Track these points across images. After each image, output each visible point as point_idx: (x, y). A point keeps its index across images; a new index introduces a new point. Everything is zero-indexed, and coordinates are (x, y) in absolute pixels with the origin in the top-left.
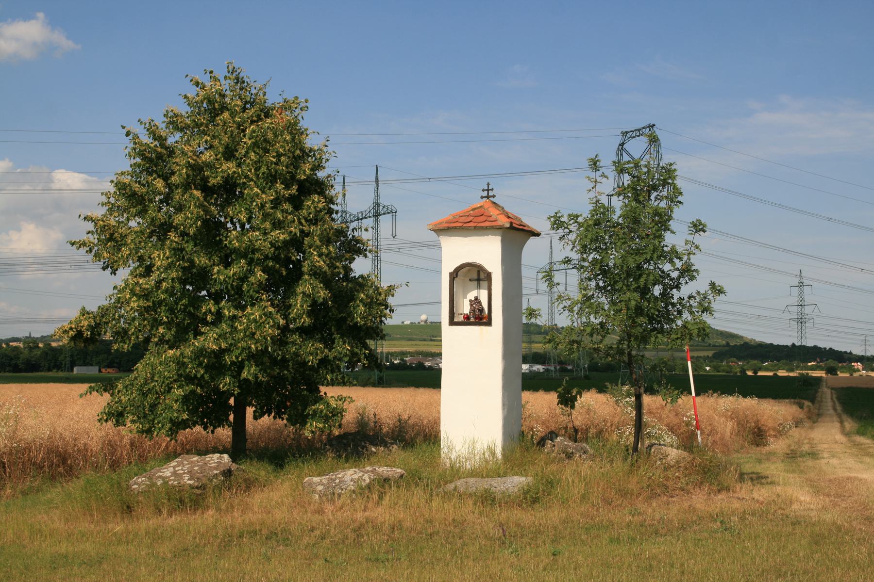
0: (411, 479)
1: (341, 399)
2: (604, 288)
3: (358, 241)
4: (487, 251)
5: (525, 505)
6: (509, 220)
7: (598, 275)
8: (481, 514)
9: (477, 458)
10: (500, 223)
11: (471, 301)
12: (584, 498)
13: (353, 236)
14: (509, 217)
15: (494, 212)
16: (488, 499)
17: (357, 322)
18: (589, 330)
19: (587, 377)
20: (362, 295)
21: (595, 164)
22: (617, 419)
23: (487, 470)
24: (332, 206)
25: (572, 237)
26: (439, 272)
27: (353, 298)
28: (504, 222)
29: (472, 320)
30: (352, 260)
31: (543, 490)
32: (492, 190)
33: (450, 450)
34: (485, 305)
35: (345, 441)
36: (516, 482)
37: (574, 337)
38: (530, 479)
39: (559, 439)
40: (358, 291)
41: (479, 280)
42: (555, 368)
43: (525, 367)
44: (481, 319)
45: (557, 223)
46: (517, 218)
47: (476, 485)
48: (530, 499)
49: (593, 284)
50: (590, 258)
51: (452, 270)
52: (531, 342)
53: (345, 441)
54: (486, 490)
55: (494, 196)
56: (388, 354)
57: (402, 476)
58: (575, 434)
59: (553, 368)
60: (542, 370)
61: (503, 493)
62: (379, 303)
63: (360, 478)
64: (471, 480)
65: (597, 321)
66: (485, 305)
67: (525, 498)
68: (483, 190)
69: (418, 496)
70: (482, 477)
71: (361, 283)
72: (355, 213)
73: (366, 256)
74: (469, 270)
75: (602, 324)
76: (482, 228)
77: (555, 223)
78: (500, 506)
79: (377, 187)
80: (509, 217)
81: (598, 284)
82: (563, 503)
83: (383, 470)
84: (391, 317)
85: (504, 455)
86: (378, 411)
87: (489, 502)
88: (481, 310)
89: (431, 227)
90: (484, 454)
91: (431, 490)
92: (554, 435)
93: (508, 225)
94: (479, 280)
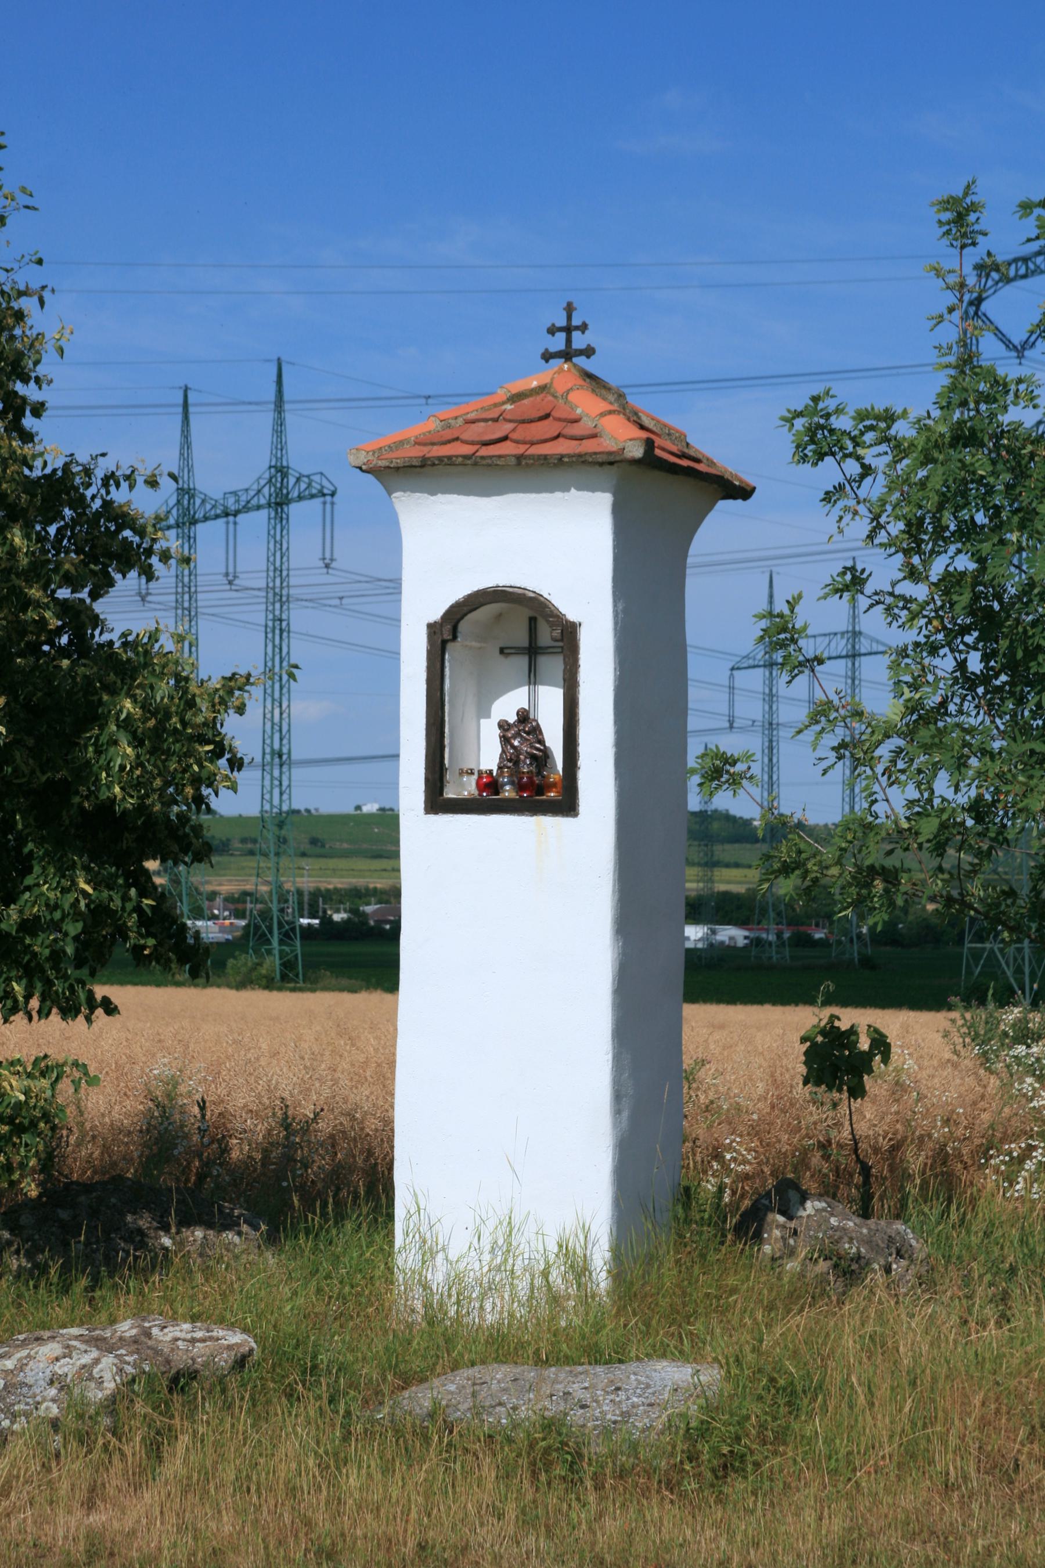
0: (278, 1374)
1: (44, 1068)
2: (985, 679)
3: (123, 519)
4: (559, 546)
5: (690, 1485)
6: (644, 435)
7: (965, 630)
8: (527, 1520)
9: (522, 1286)
10: (608, 444)
11: (503, 726)
12: (912, 1456)
13: (107, 504)
14: (642, 427)
15: (587, 405)
16: (553, 1455)
17: (113, 800)
18: (929, 827)
19: (867, 963)
20: (128, 704)
21: (960, 219)
22: (985, 1116)
23: (562, 1336)
24: (19, 387)
25: (874, 488)
26: (395, 621)
27: (93, 715)
28: (622, 438)
29: (508, 792)
30: (102, 586)
31: (762, 1426)
32: (583, 328)
33: (428, 1253)
34: (554, 740)
35: (64, 1215)
36: (664, 1386)
37: (874, 856)
38: (711, 1375)
39: (811, 1207)
40: (113, 692)
41: (533, 651)
42: (779, 935)
43: (694, 933)
44: (541, 790)
45: (818, 440)
46: (670, 433)
47: (516, 1397)
48: (714, 1457)
49: (945, 663)
50: (938, 568)
51: (436, 614)
52: (712, 864)
53: (64, 1215)
54: (550, 1425)
55: (589, 352)
56: (316, 894)
57: (241, 1362)
58: (865, 1180)
59: (772, 937)
60: (741, 942)
61: (607, 1431)
62: (186, 736)
63: (86, 1373)
64: (500, 1374)
65: (962, 799)
66: (554, 740)
67: (692, 1457)
68: (552, 331)
69: (295, 1440)
70: (540, 1362)
71: (130, 664)
72: (218, 496)
73: (148, 574)
74: (499, 617)
75: (978, 809)
76: (544, 461)
77: (812, 432)
78: (599, 1487)
79: (279, 427)
80: (642, 427)
81: (962, 665)
82: (834, 1472)
83: (178, 1337)
84: (234, 788)
85: (618, 1273)
86: (215, 1092)
87: (559, 1471)
88: (542, 759)
89: (362, 459)
90: (545, 1274)
91: (348, 1414)
92: (793, 1195)
93: (637, 451)
94: (533, 651)
